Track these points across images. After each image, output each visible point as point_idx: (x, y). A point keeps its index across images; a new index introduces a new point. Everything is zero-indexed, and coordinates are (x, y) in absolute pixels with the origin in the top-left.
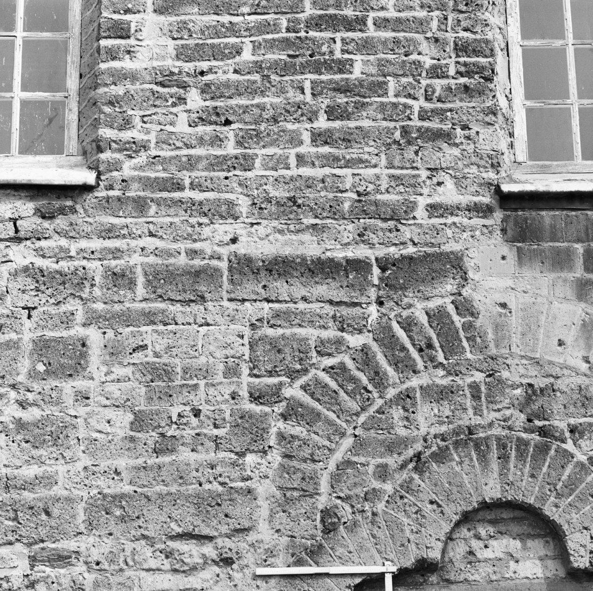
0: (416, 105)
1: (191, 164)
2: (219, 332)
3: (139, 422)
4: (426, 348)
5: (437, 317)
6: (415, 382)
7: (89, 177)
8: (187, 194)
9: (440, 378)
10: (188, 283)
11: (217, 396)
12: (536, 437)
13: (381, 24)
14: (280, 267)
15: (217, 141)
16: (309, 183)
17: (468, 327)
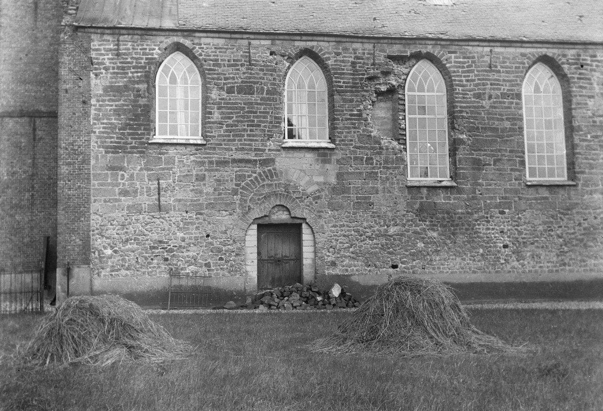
0: (267, 129)
1: (224, 140)
2: (229, 173)
3: (215, 190)
4: (267, 176)
5: (269, 170)
6: (265, 183)
7: (205, 143)
8: (223, 146)
9: (270, 182)
10: (223, 163)
11: (231, 186)
12: (286, 193)
13: (260, 112)
14: (241, 161)
15: (229, 136)
16: (246, 145)
17: (275, 173)
